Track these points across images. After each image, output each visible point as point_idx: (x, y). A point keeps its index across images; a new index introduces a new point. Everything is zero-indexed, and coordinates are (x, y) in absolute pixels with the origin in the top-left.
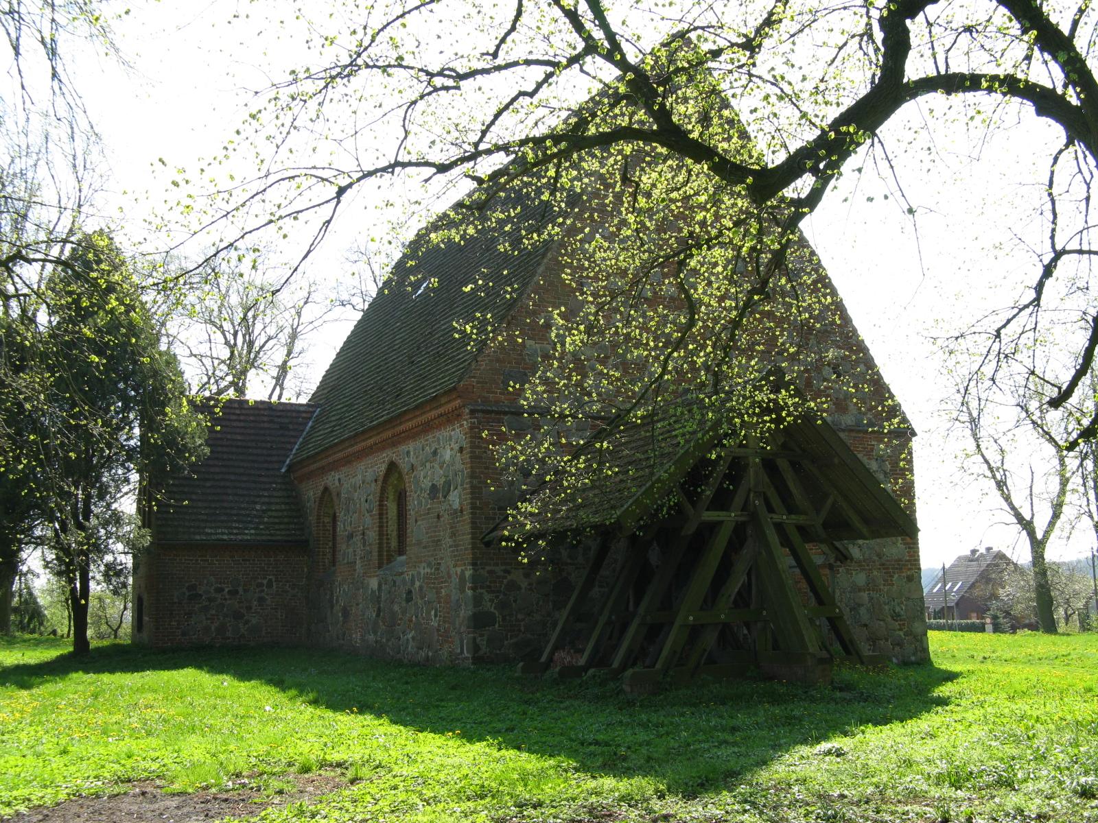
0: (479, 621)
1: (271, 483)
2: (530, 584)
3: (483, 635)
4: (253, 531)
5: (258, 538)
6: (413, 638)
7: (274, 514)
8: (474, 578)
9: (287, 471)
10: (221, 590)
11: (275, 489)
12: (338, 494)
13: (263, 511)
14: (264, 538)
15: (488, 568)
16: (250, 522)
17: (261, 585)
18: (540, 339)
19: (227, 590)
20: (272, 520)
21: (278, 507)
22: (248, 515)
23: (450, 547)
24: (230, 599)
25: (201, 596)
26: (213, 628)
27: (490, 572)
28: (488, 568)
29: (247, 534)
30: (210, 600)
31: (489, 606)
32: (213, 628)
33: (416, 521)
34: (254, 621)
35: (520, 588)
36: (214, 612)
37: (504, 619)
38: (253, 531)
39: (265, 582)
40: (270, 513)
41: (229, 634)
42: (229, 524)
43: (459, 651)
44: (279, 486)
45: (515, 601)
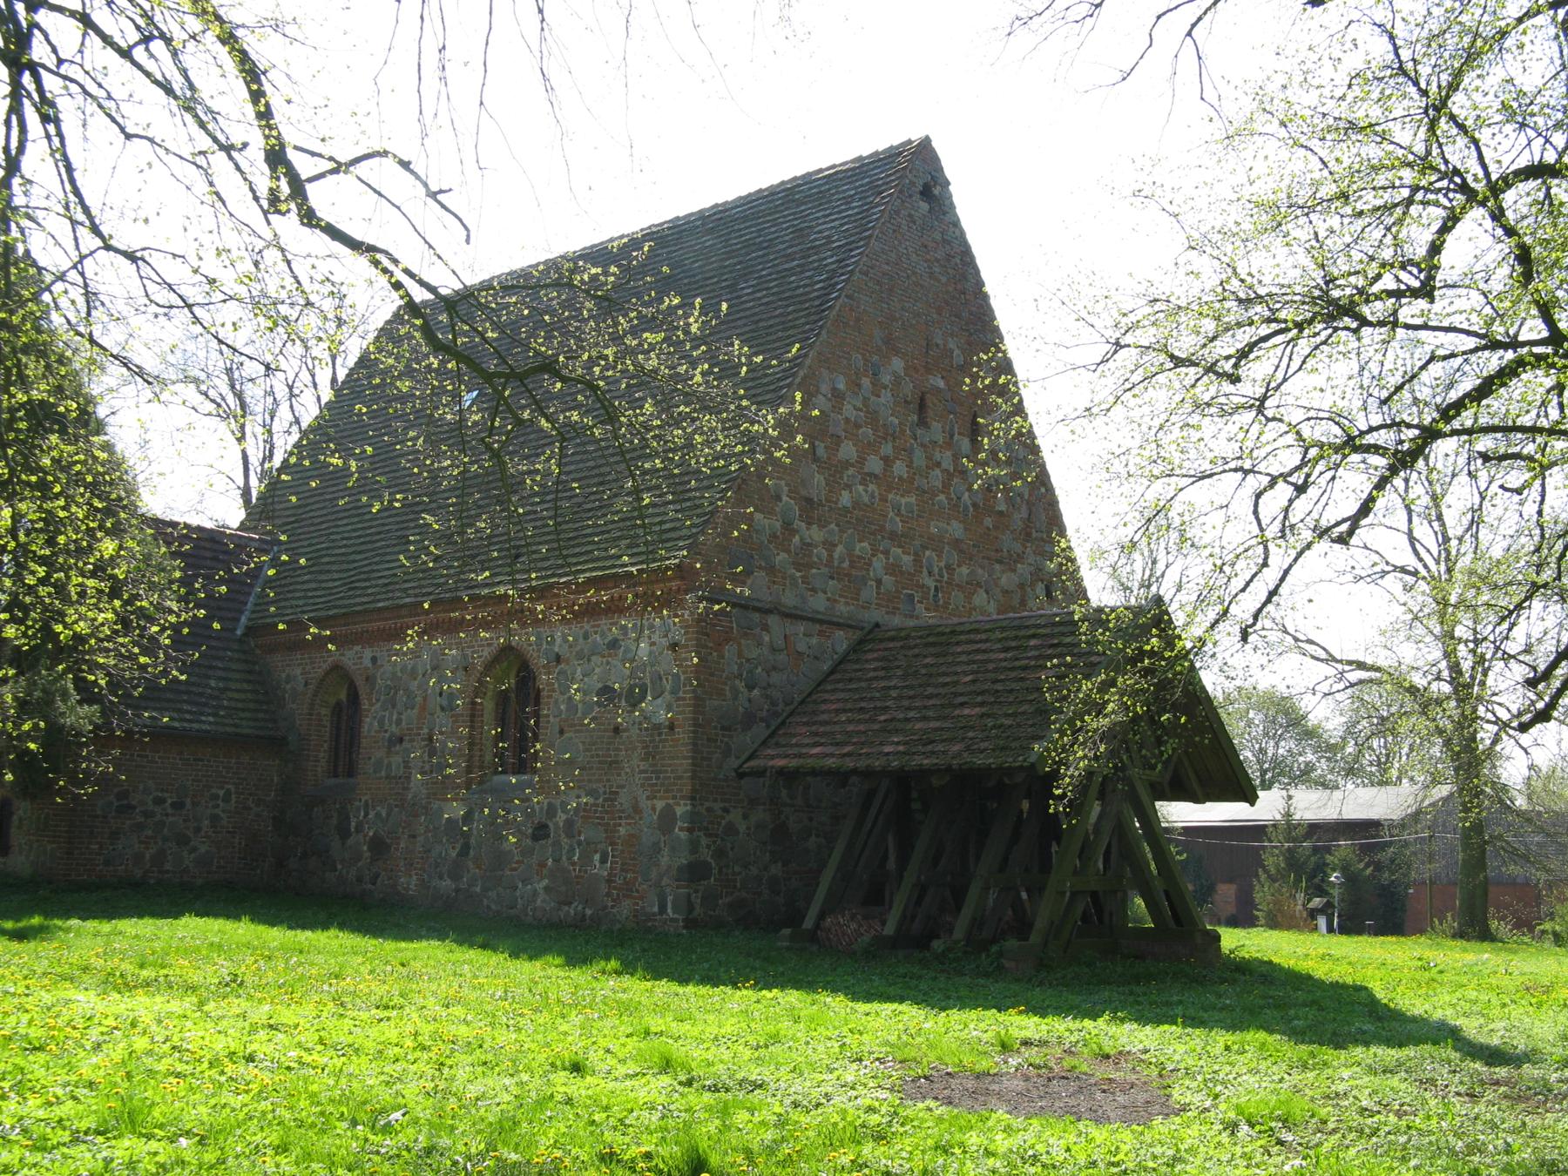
0: (695, 872)
1: (225, 649)
2: (748, 828)
3: (696, 891)
4: (211, 719)
5: (221, 729)
6: (546, 889)
7: (236, 695)
8: (693, 817)
9: (245, 635)
10: (159, 801)
11: (231, 659)
12: (370, 679)
13: (219, 689)
14: (228, 729)
15: (707, 804)
16: (205, 705)
17: (216, 797)
18: (770, 513)
19: (169, 801)
20: (233, 704)
21: (238, 686)
22: (201, 695)
23: (641, 772)
24: (173, 815)
25: (134, 808)
26: (148, 856)
27: (709, 810)
28: (707, 804)
29: (204, 722)
30: (147, 814)
31: (706, 855)
32: (148, 856)
33: (562, 732)
34: (203, 849)
35: (737, 833)
36: (150, 833)
37: (720, 871)
38: (211, 719)
39: (221, 793)
40: (230, 694)
41: (168, 867)
42: (179, 706)
43: (656, 909)
44: (236, 656)
45: (732, 849)
